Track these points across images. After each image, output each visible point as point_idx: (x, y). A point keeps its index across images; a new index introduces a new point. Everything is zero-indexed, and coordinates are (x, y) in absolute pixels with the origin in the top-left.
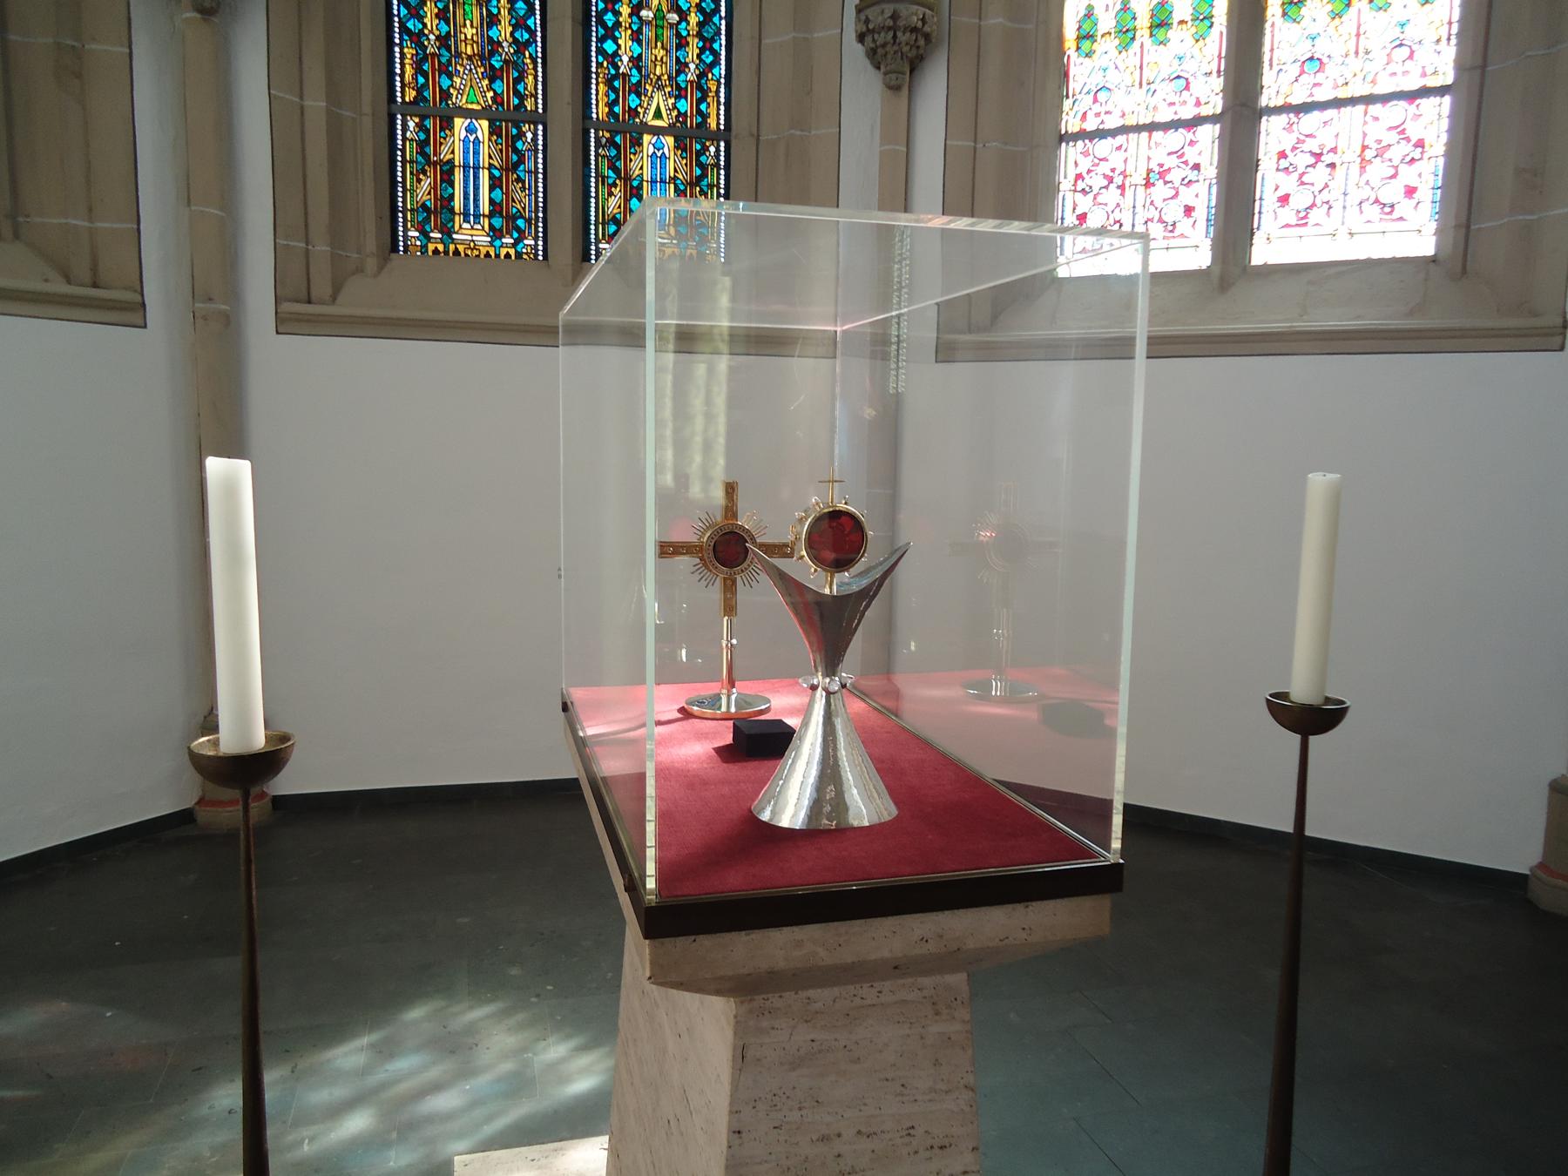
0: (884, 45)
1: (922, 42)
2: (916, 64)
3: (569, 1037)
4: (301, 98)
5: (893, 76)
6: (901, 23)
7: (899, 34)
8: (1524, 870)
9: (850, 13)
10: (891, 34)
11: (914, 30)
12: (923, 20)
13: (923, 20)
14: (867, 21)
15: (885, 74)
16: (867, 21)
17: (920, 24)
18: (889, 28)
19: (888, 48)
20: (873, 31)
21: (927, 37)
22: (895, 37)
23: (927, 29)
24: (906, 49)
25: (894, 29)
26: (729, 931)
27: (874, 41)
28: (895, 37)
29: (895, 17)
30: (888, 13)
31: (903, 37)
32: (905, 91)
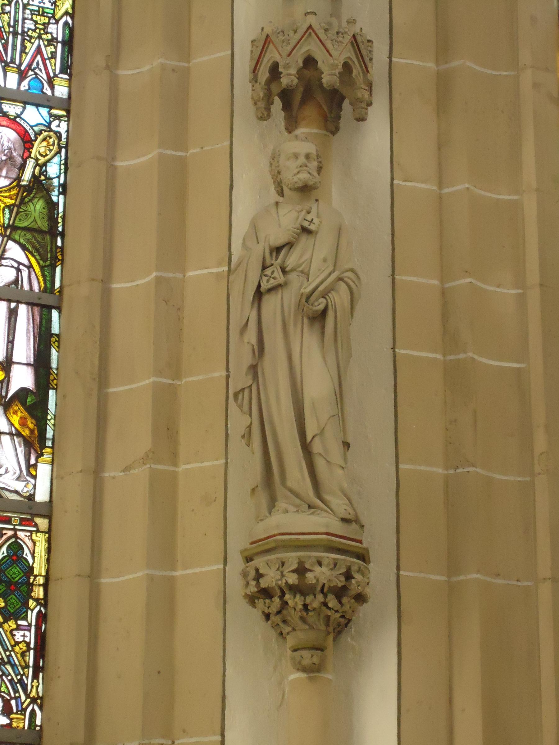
9: (236, 564)
14: (259, 576)
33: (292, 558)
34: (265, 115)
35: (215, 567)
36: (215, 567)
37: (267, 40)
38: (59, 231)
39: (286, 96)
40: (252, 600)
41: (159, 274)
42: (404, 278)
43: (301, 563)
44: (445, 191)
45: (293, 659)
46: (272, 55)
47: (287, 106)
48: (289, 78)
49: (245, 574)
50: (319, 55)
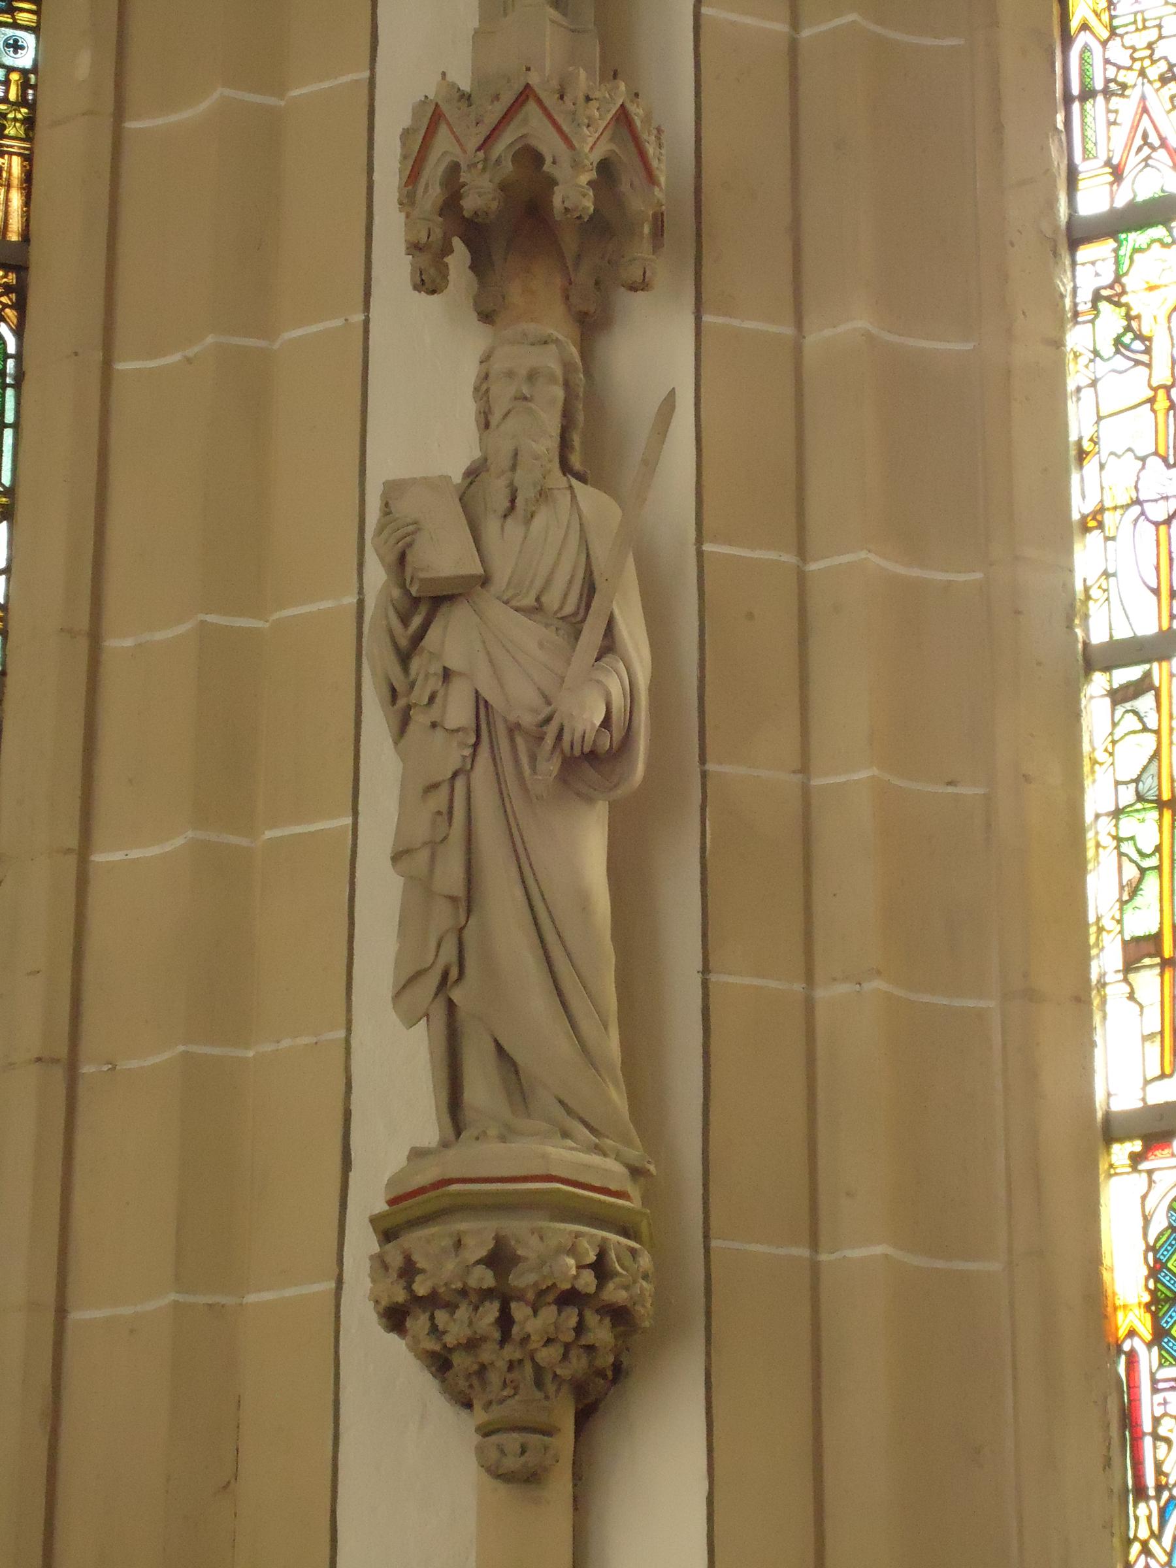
0: (472, 1344)
1: (601, 1333)
2: (596, 1398)
3: (590, 800)
4: (802, 552)
5: (512, 1441)
6: (522, 1279)
7: (519, 1311)
8: (477, 454)
9: (362, 1243)
10: (491, 1311)
11: (569, 1298)
12: (600, 1268)
13: (600, 1268)
14: (409, 1271)
15: (486, 1431)
16: (409, 1271)
17: (587, 1282)
18: (487, 1294)
19: (487, 1354)
20: (432, 1301)
21: (620, 1316)
22: (505, 1321)
23: (614, 1293)
24: (547, 1355)
25: (504, 1298)
26: (608, 853)
27: (434, 1330)
28: (505, 1321)
29: (500, 1258)
30: (477, 1249)
31: (531, 1323)
32: (561, 1485)
33: (479, 1236)
34: (429, 282)
35: (317, 1288)
36: (317, 1288)
37: (437, 117)
38: (3, 486)
39: (475, 233)
40: (395, 1318)
41: (180, 1298)
42: (773, 329)
43: (500, 1243)
44: (813, 567)
45: (480, 1451)
46: (444, 146)
47: (480, 265)
48: (480, 195)
49: (380, 1263)
50: (548, 143)
